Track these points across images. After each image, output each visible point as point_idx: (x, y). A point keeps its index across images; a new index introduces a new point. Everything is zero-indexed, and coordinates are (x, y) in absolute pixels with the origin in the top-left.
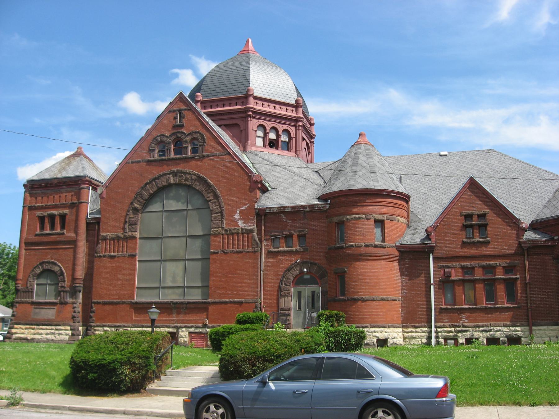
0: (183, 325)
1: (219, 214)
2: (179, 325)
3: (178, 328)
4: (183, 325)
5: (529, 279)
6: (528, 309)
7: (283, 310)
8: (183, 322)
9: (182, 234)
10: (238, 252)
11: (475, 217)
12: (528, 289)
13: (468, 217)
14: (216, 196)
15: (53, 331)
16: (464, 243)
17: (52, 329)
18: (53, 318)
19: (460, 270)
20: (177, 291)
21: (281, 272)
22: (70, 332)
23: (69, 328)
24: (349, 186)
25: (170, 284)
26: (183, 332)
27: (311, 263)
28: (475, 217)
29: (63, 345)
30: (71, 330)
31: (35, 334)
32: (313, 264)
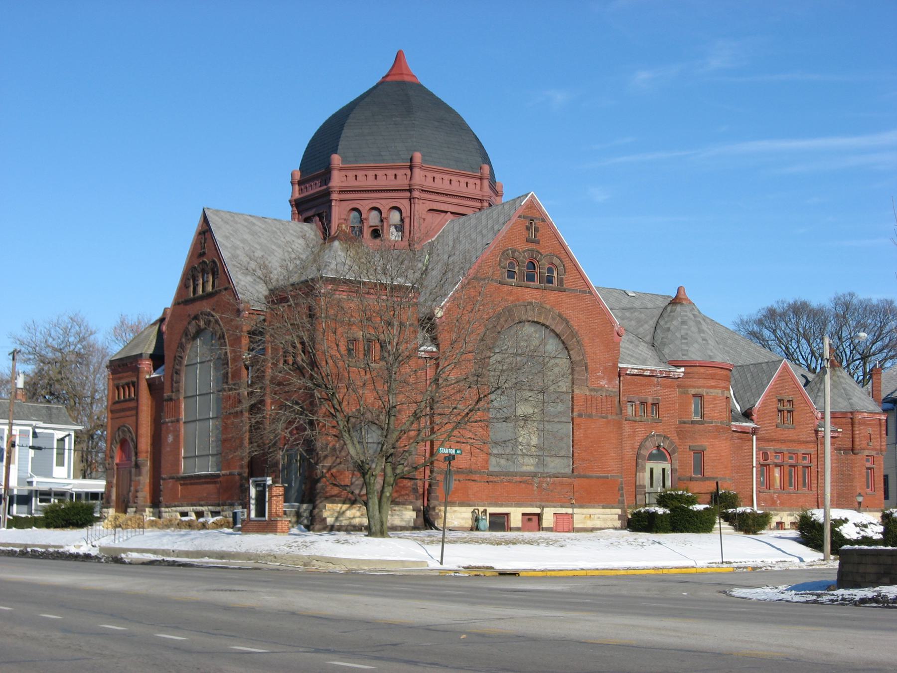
2: (543, 504)
3: (542, 507)
24: (710, 357)
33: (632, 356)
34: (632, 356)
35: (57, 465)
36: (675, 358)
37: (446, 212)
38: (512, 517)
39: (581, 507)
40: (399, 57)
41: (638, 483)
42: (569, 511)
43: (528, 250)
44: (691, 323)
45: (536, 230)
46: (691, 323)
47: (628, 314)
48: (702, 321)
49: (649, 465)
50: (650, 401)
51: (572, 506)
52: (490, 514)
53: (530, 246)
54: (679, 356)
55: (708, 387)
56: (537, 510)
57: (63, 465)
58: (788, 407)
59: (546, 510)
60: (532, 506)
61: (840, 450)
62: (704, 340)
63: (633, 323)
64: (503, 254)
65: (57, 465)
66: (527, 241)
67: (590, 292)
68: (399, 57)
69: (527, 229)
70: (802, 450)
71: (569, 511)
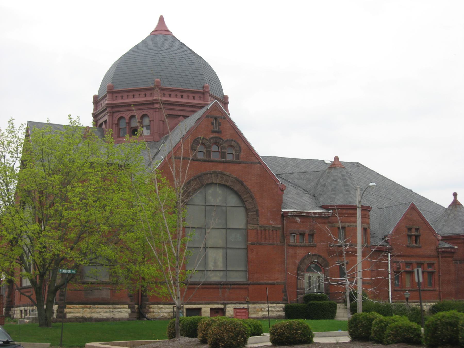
0: (229, 302)
1: (255, 213)
2: (226, 302)
3: (225, 304)
4: (229, 302)
5: (388, 256)
6: (440, 291)
7: (300, 289)
8: (229, 300)
9: (221, 226)
10: (270, 245)
11: (414, 230)
12: (441, 279)
13: (410, 229)
14: (251, 197)
15: (111, 310)
16: (407, 247)
17: (110, 308)
18: (109, 297)
19: (404, 264)
20: (218, 273)
21: (297, 261)
22: (129, 310)
23: (127, 306)
24: (350, 202)
25: (212, 268)
26: (229, 307)
27: (318, 256)
28: (414, 230)
29: (348, 344)
30: (129, 308)
31: (92, 313)
32: (319, 256)
33: (295, 203)
34: (295, 203)
35: (211, 309)
36: (326, 204)
37: (180, 116)
38: (203, 310)
39: (254, 303)
40: (161, 19)
41: (299, 287)
42: (246, 306)
43: (213, 138)
44: (340, 180)
45: (220, 124)
46: (340, 180)
47: (302, 176)
48: (347, 179)
49: (306, 275)
50: (307, 233)
51: (248, 303)
52: (187, 309)
53: (215, 135)
54: (329, 202)
55: (349, 222)
56: (221, 306)
57: (200, 310)
58: (414, 233)
59: (227, 306)
60: (218, 304)
61: (456, 260)
62: (347, 191)
63: (305, 182)
64: (194, 141)
65: (211, 309)
66: (213, 132)
67: (260, 163)
68: (161, 19)
69: (213, 124)
70: (427, 261)
71: (246, 306)
